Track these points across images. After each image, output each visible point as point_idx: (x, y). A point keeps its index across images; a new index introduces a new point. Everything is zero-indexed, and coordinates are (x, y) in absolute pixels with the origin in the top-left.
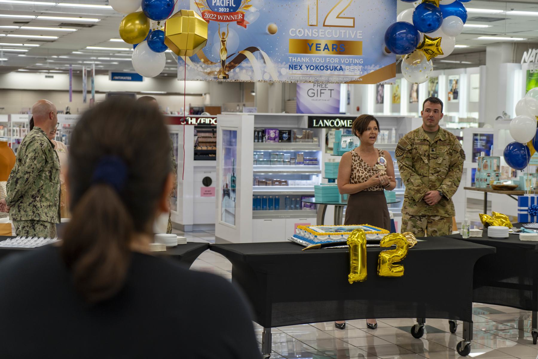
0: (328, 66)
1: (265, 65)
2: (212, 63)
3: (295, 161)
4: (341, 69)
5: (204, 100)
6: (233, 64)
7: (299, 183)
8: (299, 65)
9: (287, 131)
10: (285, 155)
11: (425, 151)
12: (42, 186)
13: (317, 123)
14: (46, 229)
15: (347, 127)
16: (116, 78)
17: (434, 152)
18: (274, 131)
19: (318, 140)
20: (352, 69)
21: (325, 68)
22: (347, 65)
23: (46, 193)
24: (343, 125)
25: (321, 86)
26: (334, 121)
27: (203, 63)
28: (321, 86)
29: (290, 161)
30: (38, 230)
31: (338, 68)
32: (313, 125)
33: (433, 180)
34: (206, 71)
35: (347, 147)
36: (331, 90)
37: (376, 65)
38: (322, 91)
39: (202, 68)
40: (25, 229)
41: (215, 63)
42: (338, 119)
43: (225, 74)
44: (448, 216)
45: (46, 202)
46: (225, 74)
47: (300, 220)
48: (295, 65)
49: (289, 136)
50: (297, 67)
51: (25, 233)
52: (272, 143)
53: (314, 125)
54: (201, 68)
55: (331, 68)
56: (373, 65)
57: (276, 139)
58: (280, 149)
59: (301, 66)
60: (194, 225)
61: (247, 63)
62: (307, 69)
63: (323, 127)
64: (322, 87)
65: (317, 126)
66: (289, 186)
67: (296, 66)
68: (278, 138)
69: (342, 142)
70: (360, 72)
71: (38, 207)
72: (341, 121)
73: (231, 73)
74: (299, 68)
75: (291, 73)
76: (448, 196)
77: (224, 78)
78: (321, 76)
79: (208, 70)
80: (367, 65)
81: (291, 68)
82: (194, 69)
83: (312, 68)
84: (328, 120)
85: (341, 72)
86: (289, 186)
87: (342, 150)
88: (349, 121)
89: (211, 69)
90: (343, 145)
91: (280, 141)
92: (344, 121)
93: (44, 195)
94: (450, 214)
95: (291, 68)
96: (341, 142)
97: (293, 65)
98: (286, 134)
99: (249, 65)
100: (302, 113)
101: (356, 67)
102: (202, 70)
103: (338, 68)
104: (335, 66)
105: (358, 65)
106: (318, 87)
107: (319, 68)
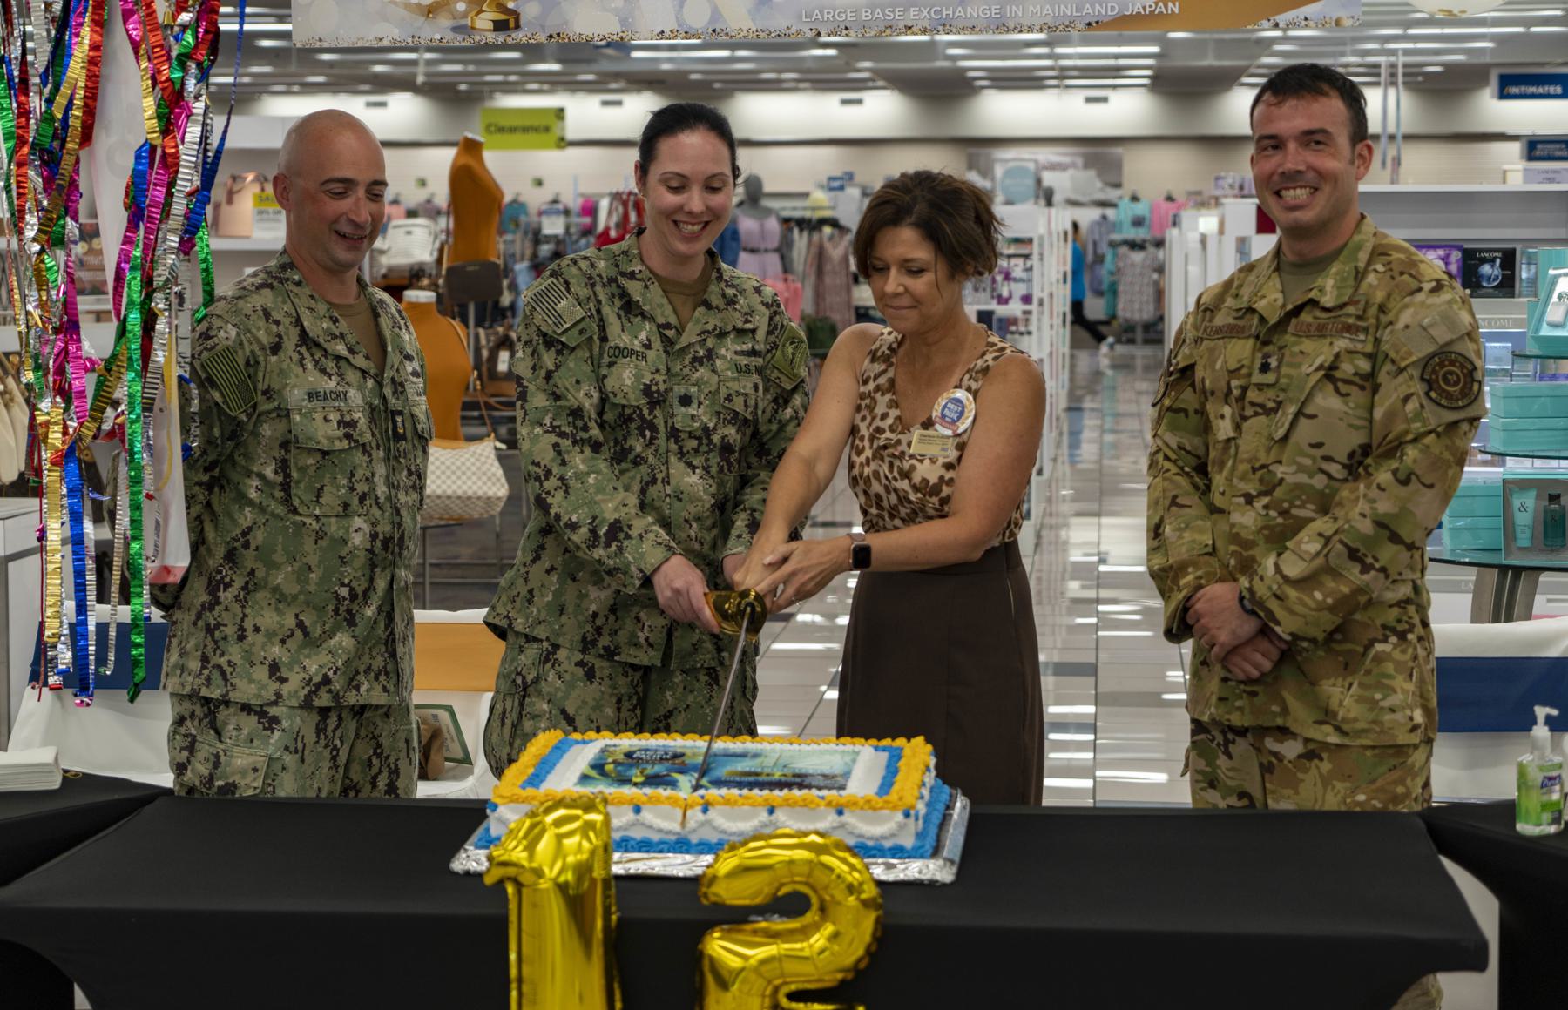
9: (1499, 255)
11: (1231, 372)
12: (245, 534)
14: (277, 734)
16: (1515, 90)
17: (1270, 378)
18: (1441, 252)
23: (272, 566)
30: (234, 733)
33: (1244, 534)
40: (183, 730)
44: (1334, 739)
45: (277, 610)
47: (1549, 601)
51: (182, 749)
71: (225, 638)
76: (1278, 623)
77: (500, 26)
87: (1546, 331)
93: (260, 574)
94: (1345, 727)
98: (1493, 266)
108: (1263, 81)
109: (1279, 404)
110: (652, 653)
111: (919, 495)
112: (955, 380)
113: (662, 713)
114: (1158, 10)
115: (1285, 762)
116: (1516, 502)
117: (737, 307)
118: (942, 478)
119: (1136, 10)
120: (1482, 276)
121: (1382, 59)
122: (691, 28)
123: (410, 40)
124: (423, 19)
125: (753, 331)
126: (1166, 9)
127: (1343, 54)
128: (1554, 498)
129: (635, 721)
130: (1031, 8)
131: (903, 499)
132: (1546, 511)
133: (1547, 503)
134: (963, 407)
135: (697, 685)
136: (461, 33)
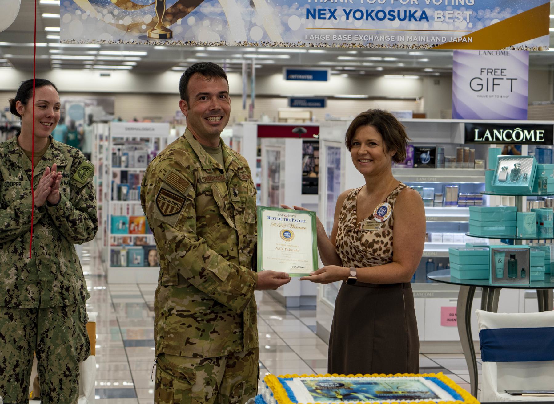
0: (394, 12)
1: (253, 10)
2: (135, 6)
3: (443, 200)
4: (424, 17)
5: (419, 105)
6: (181, 7)
7: (450, 237)
8: (330, 10)
10: (426, 189)
13: (481, 135)
15: (536, 143)
16: (293, 76)
19: (484, 165)
20: (449, 18)
21: (388, 16)
22: (437, 8)
24: (528, 137)
25: (493, 73)
26: (511, 131)
27: (114, 6)
28: (493, 73)
29: (434, 199)
31: (416, 15)
32: (474, 138)
34: (121, 22)
35: (509, 179)
36: (512, 79)
37: (503, 9)
38: (496, 82)
39: (114, 16)
41: (142, 6)
42: (518, 128)
43: (164, 28)
46: (164, 28)
47: (451, 300)
48: (320, 10)
49: (432, 157)
50: (324, 14)
52: (402, 169)
53: (476, 139)
54: (111, 15)
55: (402, 16)
56: (497, 9)
57: (409, 162)
58: (415, 179)
59: (333, 10)
60: (302, 297)
61: (213, 5)
62: (348, 19)
63: (492, 142)
64: (495, 75)
65: (481, 139)
66: (432, 243)
67: (322, 12)
68: (412, 161)
69: (500, 170)
70: (468, 23)
72: (524, 133)
73: (177, 27)
74: (328, 15)
75: (310, 26)
77: (162, 37)
78: (378, 33)
79: (127, 21)
80: (484, 9)
81: (310, 16)
82: (96, 19)
83: (358, 15)
84: (501, 131)
85: (424, 25)
86: (432, 243)
87: (498, 184)
88: (538, 132)
89: (133, 18)
90: (501, 175)
91: (416, 165)
92: (529, 133)
95: (310, 16)
96: (497, 170)
97: (315, 10)
98: (426, 154)
99: (217, 10)
100: (461, 118)
101: (457, 13)
102: (113, 22)
103: (418, 15)
104: (410, 12)
105: (463, 8)
106: (489, 74)
107: (373, 14)
108: (185, 69)
109: (243, 209)
110: (35, 303)
111: (364, 248)
112: (383, 199)
113: (44, 330)
114: (463, 40)
115: (240, 360)
116: (497, 259)
117: (59, 158)
118: (374, 240)
119: (454, 40)
120: (422, 159)
121: (243, 62)
122: (253, 41)
123: (368, 45)
124: (125, 32)
125: (65, 167)
126: (467, 40)
127: (225, 59)
128: (513, 256)
129: (34, 333)
130: (408, 37)
131: (357, 251)
132: (509, 262)
133: (509, 258)
134: (386, 210)
135: (58, 318)
136: (143, 40)
